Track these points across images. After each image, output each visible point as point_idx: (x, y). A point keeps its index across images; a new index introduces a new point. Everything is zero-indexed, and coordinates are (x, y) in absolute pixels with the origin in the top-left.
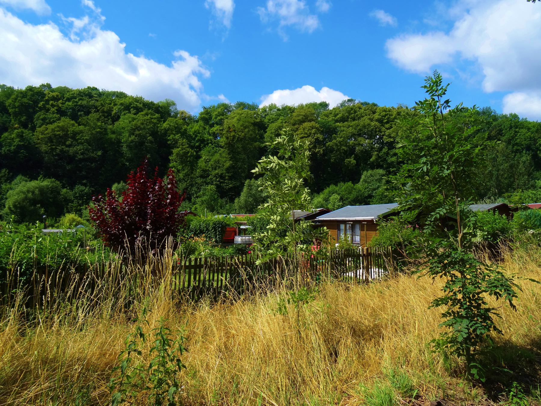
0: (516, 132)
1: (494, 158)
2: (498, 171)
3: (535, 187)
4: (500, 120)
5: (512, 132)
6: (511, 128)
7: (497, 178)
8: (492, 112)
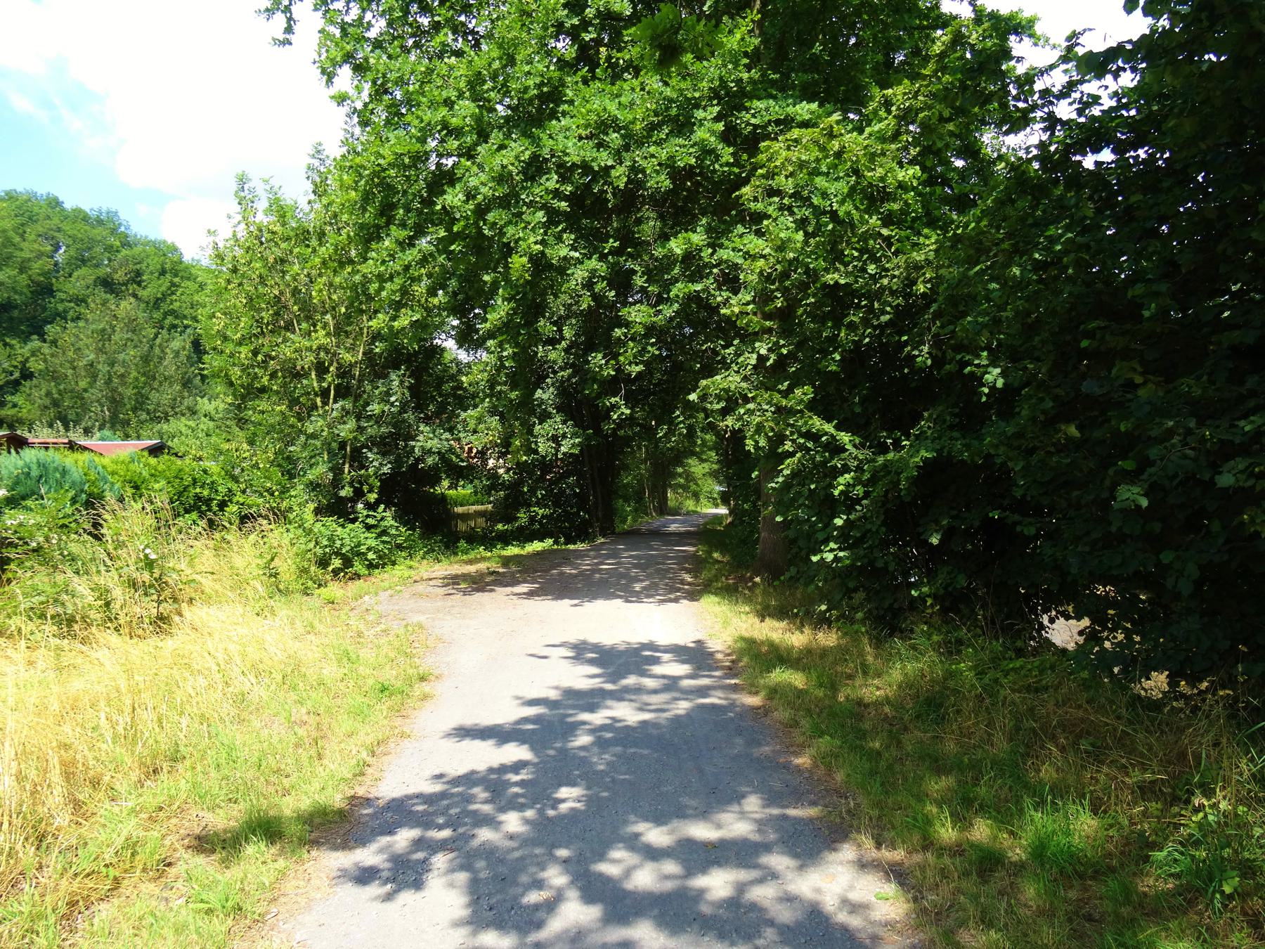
0: (173, 284)
1: (104, 330)
2: (112, 364)
3: (194, 413)
4: (140, 248)
5: (165, 282)
6: (163, 272)
7: (109, 381)
8: (120, 225)
